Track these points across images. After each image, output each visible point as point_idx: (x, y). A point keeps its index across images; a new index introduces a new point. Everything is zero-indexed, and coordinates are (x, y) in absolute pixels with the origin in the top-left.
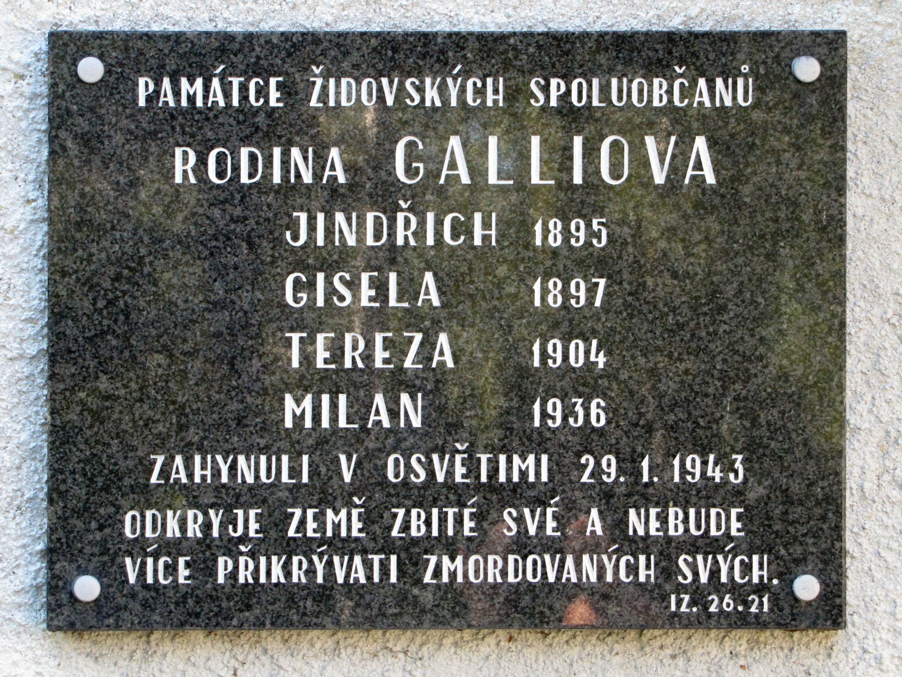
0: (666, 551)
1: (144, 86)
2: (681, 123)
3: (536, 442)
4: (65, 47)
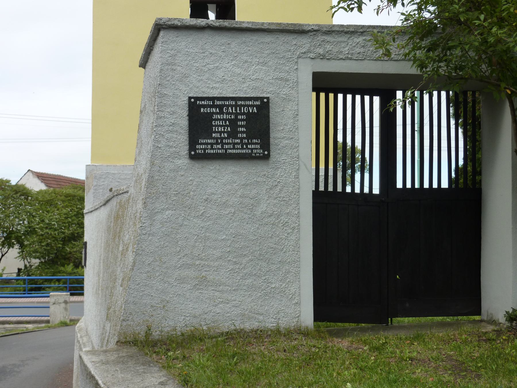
0: (252, 149)
1: (198, 102)
2: (252, 106)
3: (239, 138)
4: (190, 98)
